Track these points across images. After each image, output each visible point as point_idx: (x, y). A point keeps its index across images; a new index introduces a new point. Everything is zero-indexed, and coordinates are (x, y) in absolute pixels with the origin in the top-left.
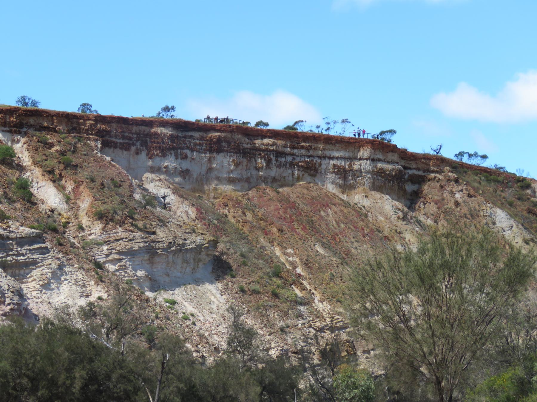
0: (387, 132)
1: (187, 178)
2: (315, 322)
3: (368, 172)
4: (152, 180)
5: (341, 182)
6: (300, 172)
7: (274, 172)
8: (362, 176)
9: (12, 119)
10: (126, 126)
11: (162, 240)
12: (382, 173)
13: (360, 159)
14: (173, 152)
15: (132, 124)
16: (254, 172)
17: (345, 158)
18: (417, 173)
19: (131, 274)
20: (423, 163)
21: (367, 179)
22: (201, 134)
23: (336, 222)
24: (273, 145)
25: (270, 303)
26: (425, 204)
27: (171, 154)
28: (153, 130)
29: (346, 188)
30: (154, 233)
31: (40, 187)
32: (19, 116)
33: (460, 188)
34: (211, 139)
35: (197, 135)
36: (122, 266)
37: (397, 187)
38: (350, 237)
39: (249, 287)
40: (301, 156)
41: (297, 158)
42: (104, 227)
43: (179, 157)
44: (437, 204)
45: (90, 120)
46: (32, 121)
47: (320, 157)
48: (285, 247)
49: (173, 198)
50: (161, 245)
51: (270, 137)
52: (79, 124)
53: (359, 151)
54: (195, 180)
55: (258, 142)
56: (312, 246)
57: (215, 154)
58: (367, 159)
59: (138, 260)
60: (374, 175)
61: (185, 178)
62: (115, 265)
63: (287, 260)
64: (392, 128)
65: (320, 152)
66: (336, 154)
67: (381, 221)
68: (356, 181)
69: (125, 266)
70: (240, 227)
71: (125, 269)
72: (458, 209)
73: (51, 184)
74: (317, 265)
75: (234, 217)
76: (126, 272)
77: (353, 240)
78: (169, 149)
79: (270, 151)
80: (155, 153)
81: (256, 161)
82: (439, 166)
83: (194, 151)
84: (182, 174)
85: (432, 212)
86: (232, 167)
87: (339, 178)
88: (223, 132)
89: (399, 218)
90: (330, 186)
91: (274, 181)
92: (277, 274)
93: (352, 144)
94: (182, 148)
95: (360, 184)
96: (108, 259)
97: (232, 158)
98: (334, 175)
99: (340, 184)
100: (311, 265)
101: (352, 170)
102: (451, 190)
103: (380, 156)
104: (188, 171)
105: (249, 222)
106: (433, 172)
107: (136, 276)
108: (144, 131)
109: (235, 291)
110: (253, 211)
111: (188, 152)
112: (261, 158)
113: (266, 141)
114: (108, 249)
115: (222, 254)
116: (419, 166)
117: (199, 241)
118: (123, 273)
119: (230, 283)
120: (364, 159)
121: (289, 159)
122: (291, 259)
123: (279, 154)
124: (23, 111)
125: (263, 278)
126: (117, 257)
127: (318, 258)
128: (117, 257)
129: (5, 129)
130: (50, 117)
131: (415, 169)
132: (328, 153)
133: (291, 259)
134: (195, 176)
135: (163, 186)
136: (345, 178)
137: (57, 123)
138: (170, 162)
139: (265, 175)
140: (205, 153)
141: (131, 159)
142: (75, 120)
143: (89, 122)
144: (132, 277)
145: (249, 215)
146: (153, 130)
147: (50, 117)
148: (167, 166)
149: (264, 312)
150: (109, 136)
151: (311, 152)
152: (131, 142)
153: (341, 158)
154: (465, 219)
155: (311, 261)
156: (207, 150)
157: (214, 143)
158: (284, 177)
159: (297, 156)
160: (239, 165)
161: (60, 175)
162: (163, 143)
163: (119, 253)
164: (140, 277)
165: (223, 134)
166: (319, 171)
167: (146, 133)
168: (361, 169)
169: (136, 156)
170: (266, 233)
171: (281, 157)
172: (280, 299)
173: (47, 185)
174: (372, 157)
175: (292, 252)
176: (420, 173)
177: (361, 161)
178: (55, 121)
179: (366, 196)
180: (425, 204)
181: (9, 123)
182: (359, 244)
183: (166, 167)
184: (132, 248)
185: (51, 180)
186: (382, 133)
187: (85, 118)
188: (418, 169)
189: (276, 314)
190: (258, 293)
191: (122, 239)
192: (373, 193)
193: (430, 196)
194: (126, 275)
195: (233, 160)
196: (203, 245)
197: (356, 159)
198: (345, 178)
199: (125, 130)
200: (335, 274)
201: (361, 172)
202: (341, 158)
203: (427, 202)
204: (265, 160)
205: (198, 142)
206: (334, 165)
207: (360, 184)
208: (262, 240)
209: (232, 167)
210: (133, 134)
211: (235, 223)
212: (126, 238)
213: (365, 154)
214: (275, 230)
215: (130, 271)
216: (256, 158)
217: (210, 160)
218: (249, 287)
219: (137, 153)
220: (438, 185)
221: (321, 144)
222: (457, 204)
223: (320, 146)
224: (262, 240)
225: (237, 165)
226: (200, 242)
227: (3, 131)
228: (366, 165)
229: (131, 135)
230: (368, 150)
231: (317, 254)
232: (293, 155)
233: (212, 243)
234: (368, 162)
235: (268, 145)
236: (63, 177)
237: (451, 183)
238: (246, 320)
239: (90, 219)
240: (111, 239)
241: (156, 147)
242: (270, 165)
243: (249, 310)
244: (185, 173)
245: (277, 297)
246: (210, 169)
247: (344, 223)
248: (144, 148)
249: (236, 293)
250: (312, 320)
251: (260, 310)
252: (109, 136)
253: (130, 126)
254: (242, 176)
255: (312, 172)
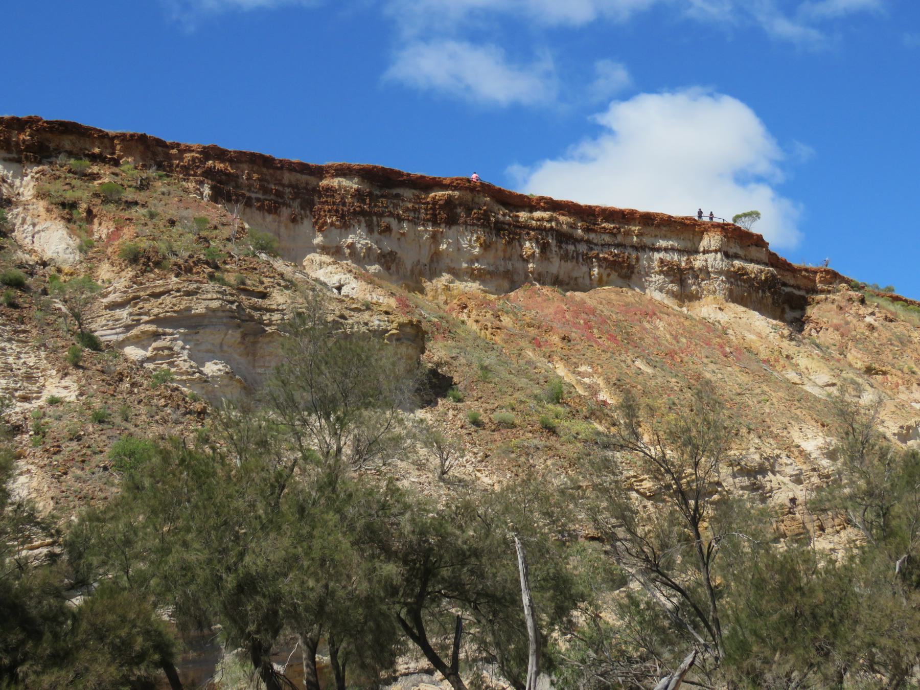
0: (745, 215)
1: (393, 268)
2: (642, 481)
3: (720, 272)
4: (321, 265)
5: (675, 288)
6: (602, 270)
7: (556, 266)
8: (709, 278)
9: (22, 137)
10: (271, 171)
11: (280, 307)
12: (743, 275)
13: (705, 252)
14: (362, 219)
15: (281, 168)
16: (519, 265)
17: (681, 252)
18: (797, 292)
19: (185, 367)
20: (804, 277)
21: (718, 284)
22: (416, 192)
23: (671, 334)
24: (550, 220)
25: (536, 442)
26: (818, 332)
27: (359, 222)
28: (324, 183)
29: (685, 296)
30: (264, 296)
31: (39, 232)
32: (37, 130)
33: (870, 310)
34: (435, 202)
35: (408, 193)
36: (162, 349)
37: (770, 300)
38: (699, 355)
39: (492, 416)
40: (602, 245)
41: (596, 248)
42: (136, 276)
43: (376, 229)
44: (838, 330)
45: (193, 151)
46: (67, 143)
47: (635, 248)
48: (575, 363)
49: (354, 285)
50: (276, 317)
51: (545, 210)
52: (169, 157)
53: (701, 239)
54: (409, 273)
55: (523, 215)
56: (629, 362)
57: (443, 226)
58: (716, 251)
59: (210, 337)
60: (731, 277)
61: (388, 269)
62: (145, 348)
63: (579, 382)
64: (753, 210)
65: (635, 239)
66: (662, 243)
67: (751, 340)
68: (700, 287)
69: (170, 349)
70: (489, 336)
71: (171, 356)
72: (876, 335)
73: (60, 224)
74: (639, 387)
75: (477, 321)
76: (172, 364)
77: (705, 360)
78: (355, 214)
79: (545, 229)
80: (329, 221)
81: (521, 246)
82: (831, 283)
83: (404, 220)
84: (383, 260)
85: (832, 342)
86: (477, 250)
87: (672, 282)
88: (455, 188)
89: (782, 336)
90: (656, 292)
91: (558, 282)
92: (557, 398)
93: (688, 230)
94: (381, 215)
95: (709, 291)
96: (129, 334)
97: (475, 235)
98: (662, 277)
99: (673, 292)
100: (628, 386)
101: (692, 268)
102: (857, 313)
103: (734, 249)
104: (392, 254)
105: (505, 328)
106: (822, 292)
107: (201, 372)
108: (307, 184)
109: (459, 424)
110: (515, 314)
111: (394, 223)
112: (530, 240)
113: (538, 214)
114: (130, 314)
115: (439, 364)
116: (799, 283)
117: (377, 322)
118: (165, 366)
119: (451, 412)
120: (711, 252)
121: (582, 248)
122: (587, 380)
123: (563, 238)
124: (47, 122)
125: (525, 402)
126: (152, 328)
127: (640, 377)
128: (152, 328)
129: (10, 156)
130: (106, 140)
131: (792, 286)
132: (647, 240)
133: (587, 380)
134: (409, 267)
135: (340, 269)
136: (682, 282)
137: (120, 150)
138: (358, 238)
139: (540, 269)
140: (423, 225)
141: (283, 230)
142: (160, 149)
143: (188, 156)
144: (188, 373)
145: (506, 320)
146: (324, 183)
147: (106, 140)
148: (352, 244)
149: (523, 459)
150: (233, 183)
151: (620, 239)
152: (280, 200)
153: (673, 249)
154: (891, 347)
155: (628, 381)
156: (428, 220)
157: (441, 207)
158: (576, 279)
159: (596, 245)
160: (489, 246)
161: (89, 212)
162: (344, 204)
163: (157, 321)
164: (213, 377)
165: (457, 193)
166: (636, 270)
167: (309, 187)
168: (707, 267)
169: (291, 225)
170: (537, 343)
171: (567, 243)
172: (558, 436)
173: (54, 227)
174: (725, 249)
175: (590, 370)
176: (802, 293)
177: (706, 255)
178: (118, 147)
179: (720, 309)
180: (818, 332)
181: (17, 143)
182: (718, 366)
183: (351, 246)
184: (189, 309)
185: (63, 218)
186: (736, 218)
187: (182, 147)
188: (798, 288)
189: (549, 462)
190: (513, 426)
191: (168, 292)
192: (732, 305)
193: (825, 320)
194: (173, 370)
195: (478, 238)
196: (387, 331)
197: (697, 252)
198: (682, 282)
199: (268, 177)
200: (677, 401)
201: (709, 273)
202: (673, 249)
203: (821, 328)
204: (537, 242)
205: (410, 205)
206: (662, 261)
207: (709, 291)
208: (530, 353)
209: (477, 250)
210: (284, 186)
211: (478, 331)
212: (178, 290)
213: (712, 242)
214: (555, 339)
215: (183, 362)
216: (522, 240)
217: (434, 237)
218: (492, 416)
219: (294, 221)
220: (834, 307)
221: (635, 226)
222: (872, 328)
223: (633, 228)
224: (530, 353)
225: (486, 246)
226: (379, 326)
227: (5, 160)
228: (715, 261)
229: (281, 189)
230: (716, 237)
231: (639, 372)
232: (588, 242)
233: (408, 330)
234: (719, 255)
235: (542, 219)
236: (96, 216)
237: (855, 304)
238: (479, 474)
239: (114, 268)
240: (142, 294)
241: (329, 211)
242: (548, 253)
243: (487, 456)
244: (388, 260)
245: (554, 432)
246: (436, 256)
247: (686, 337)
248: (308, 212)
249: (462, 427)
250: (634, 477)
251: (513, 456)
252: (233, 183)
253: (279, 172)
254: (497, 268)
255: (624, 271)
